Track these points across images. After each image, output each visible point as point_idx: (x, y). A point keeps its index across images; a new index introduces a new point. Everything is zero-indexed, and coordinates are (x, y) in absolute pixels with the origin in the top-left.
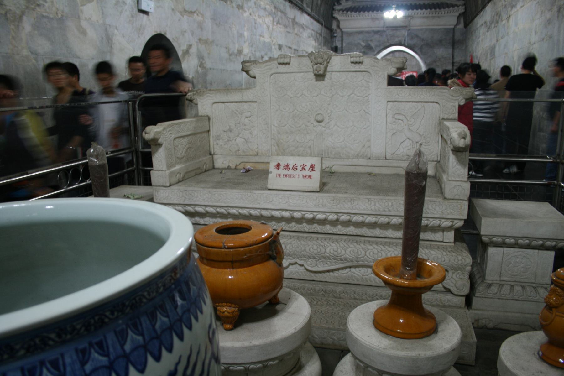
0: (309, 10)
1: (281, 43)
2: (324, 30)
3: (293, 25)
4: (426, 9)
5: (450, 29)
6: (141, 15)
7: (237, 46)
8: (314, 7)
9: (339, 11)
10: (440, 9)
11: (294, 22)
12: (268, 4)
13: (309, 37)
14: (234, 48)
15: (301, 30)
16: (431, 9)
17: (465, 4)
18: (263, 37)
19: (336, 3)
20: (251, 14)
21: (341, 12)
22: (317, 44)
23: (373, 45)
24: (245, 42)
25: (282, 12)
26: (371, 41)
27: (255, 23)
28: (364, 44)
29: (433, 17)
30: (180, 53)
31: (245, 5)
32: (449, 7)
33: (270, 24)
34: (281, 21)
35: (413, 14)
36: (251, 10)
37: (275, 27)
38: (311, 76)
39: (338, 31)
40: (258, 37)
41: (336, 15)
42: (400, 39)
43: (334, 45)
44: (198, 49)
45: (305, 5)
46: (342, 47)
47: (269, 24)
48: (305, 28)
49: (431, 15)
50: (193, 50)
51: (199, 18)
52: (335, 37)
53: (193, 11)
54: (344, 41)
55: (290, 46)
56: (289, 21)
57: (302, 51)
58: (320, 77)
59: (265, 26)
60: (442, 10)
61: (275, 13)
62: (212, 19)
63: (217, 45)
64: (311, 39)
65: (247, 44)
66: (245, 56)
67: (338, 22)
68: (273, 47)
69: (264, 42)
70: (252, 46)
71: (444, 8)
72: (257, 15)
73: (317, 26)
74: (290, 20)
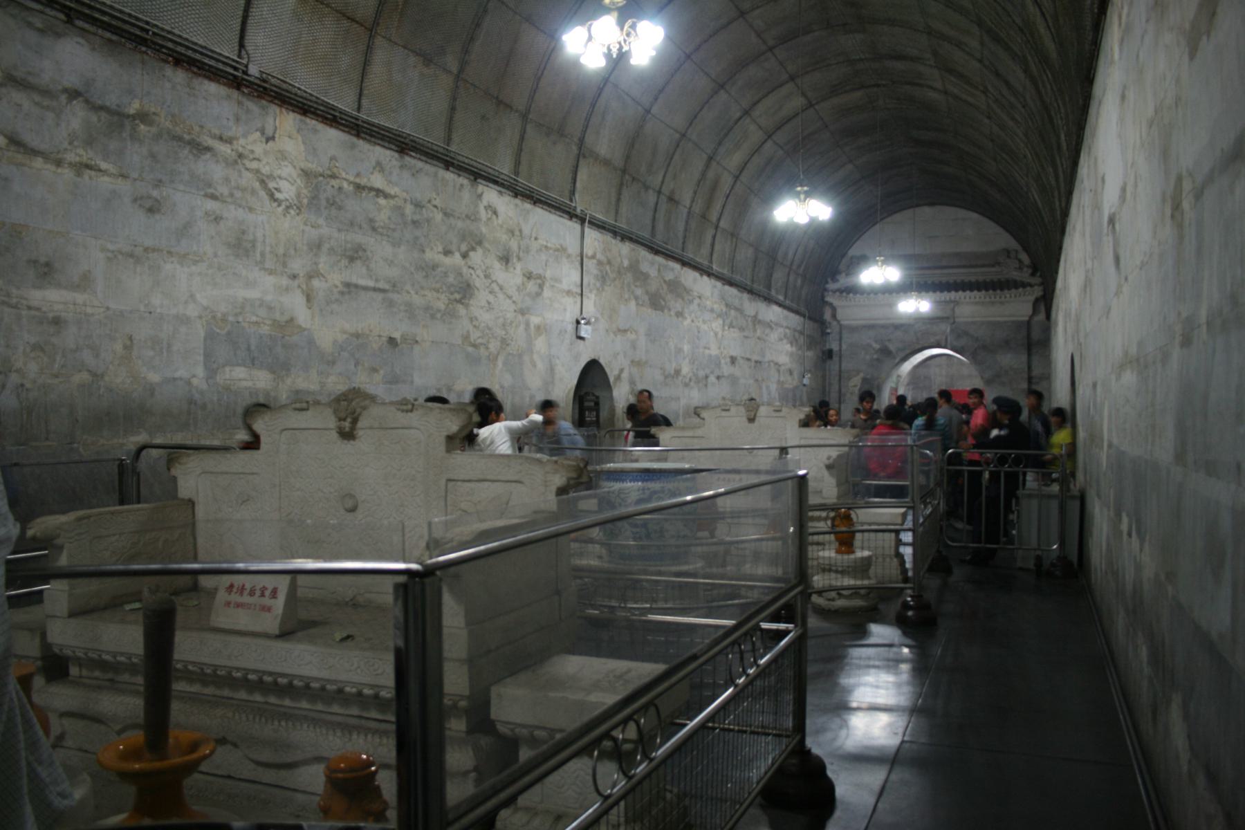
0: (781, 298)
1: (734, 354)
2: (810, 325)
3: (754, 325)
4: (979, 290)
5: (1022, 322)
6: (579, 341)
7: (674, 365)
8: (790, 293)
9: (834, 292)
10: (1002, 289)
11: (756, 321)
12: (716, 303)
13: (781, 340)
14: (670, 369)
15: (768, 331)
16: (987, 290)
17: (1042, 284)
18: (709, 349)
19: (829, 280)
20: (693, 321)
21: (838, 293)
22: (794, 349)
23: (892, 347)
24: (684, 358)
25: (737, 309)
26: (889, 340)
27: (699, 332)
28: (877, 346)
29: (993, 303)
30: (612, 379)
31: (686, 310)
32: (1016, 288)
33: (719, 330)
34: (734, 323)
35: (958, 298)
36: (693, 315)
37: (726, 332)
38: (745, 419)
39: (835, 323)
40: (701, 350)
41: (829, 299)
42: (938, 338)
43: (828, 347)
44: (630, 373)
45: (773, 293)
46: (840, 350)
47: (717, 330)
48: (773, 326)
49: (988, 299)
50: (625, 375)
51: (633, 336)
52: (829, 334)
53: (626, 328)
54: (843, 342)
55: (748, 356)
56: (747, 321)
57: (769, 362)
58: (751, 420)
59: (712, 334)
60: (1006, 291)
61: (726, 313)
62: (646, 335)
63: (650, 366)
64: (785, 341)
65: (687, 360)
66: (684, 377)
67: (834, 309)
68: (723, 361)
69: (710, 356)
70: (693, 363)
71: (1009, 289)
72: (701, 320)
73: (794, 320)
74: (750, 319)
